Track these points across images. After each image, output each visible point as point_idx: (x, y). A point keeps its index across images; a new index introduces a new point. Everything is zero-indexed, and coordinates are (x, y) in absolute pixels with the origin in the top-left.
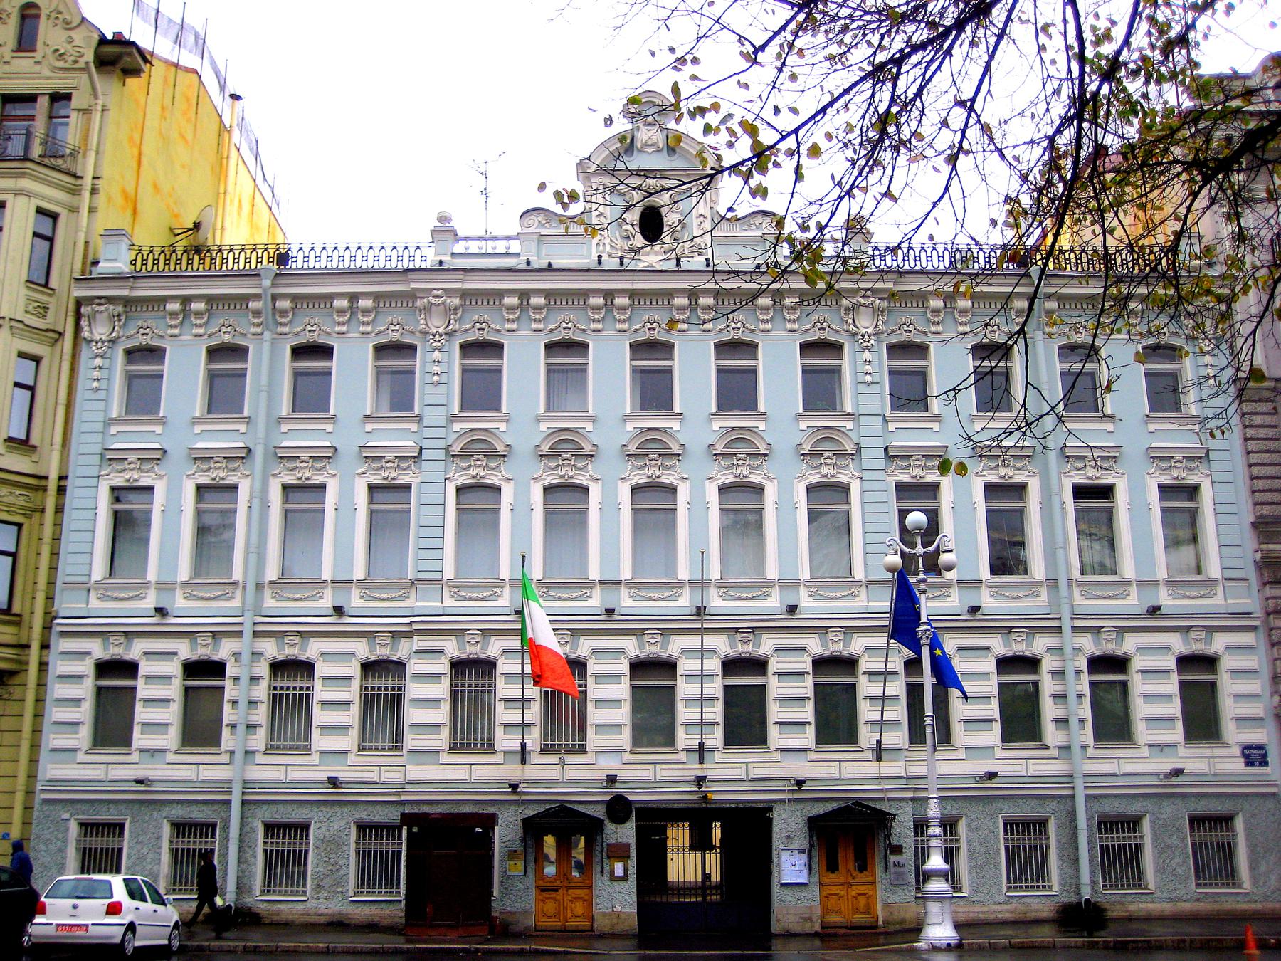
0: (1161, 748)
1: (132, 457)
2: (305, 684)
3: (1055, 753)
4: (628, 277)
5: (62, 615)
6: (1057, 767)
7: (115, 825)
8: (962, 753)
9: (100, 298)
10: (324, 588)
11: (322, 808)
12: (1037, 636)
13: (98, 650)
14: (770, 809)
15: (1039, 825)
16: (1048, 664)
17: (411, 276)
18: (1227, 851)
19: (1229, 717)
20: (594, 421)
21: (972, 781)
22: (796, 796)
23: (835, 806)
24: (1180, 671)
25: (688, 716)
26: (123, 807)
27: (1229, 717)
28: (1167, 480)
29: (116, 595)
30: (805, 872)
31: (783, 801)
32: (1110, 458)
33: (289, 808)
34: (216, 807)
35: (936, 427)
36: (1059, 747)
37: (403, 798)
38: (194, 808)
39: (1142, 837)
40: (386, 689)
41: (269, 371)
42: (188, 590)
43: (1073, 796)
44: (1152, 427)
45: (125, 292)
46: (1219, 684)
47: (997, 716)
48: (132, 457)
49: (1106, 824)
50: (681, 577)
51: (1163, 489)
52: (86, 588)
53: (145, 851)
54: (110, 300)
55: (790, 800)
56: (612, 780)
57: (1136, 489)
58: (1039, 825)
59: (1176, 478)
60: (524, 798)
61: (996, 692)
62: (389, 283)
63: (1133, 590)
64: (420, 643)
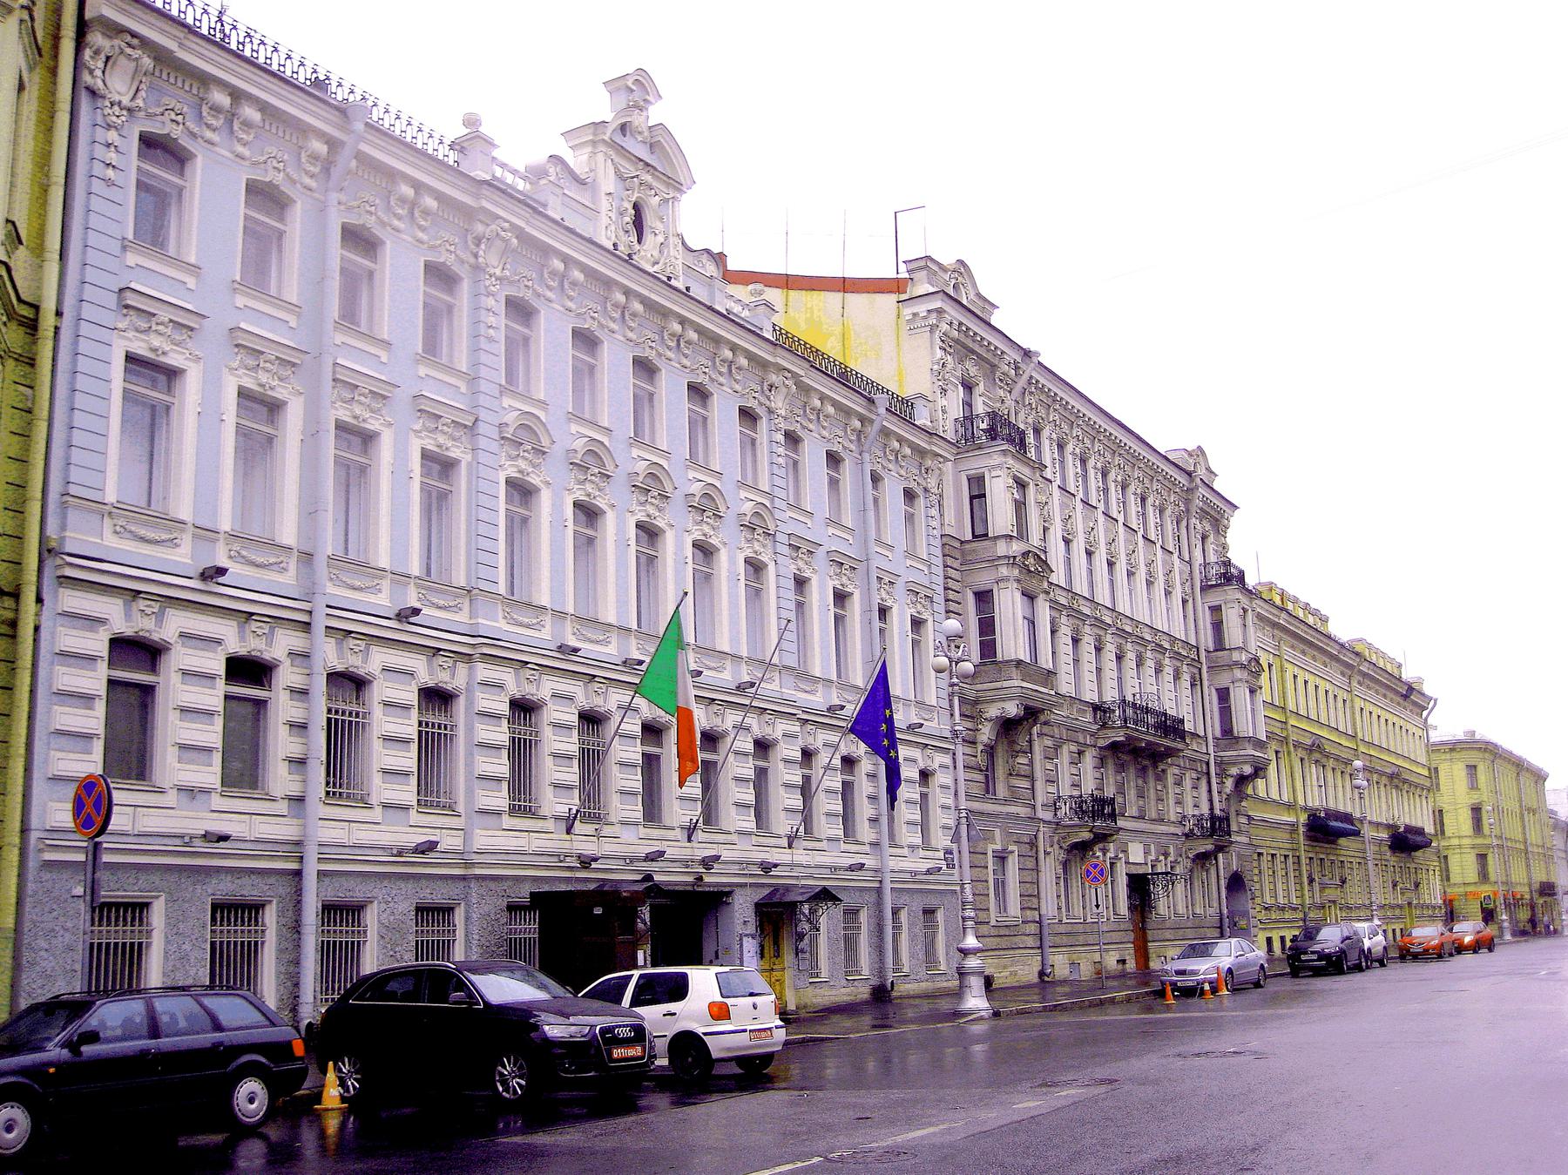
0: (190, 792)
1: (164, 315)
2: (355, 708)
3: (282, 807)
4: (627, 270)
5: (67, 550)
6: (284, 830)
7: (134, 906)
8: (171, 798)
9: (134, 35)
10: (183, 530)
11: (386, 883)
12: (170, 612)
13: (120, 619)
14: (729, 894)
15: (251, 910)
16: (287, 676)
17: (935, 440)
18: (251, 952)
19: (281, 754)
20: (198, 276)
21: (178, 841)
22: (579, 875)
23: (592, 886)
24: (112, 664)
25: (624, 783)
26: (156, 878)
27: (170, 741)
28: (249, 383)
29: (142, 532)
30: (43, 996)
31: (745, 885)
32: (186, 326)
33: (351, 883)
34: (272, 880)
35: (191, 282)
36: (290, 799)
37: (470, 872)
38: (246, 880)
39: (149, 932)
40: (344, 713)
41: (479, 315)
42: (236, 547)
43: (298, 874)
44: (241, 301)
45: (172, 45)
46: (271, 706)
47: (101, 731)
48: (164, 315)
49: (332, 911)
50: (183, 516)
51: (243, 394)
52: (98, 507)
53: (187, 947)
54: (145, 43)
55: (751, 885)
56: (767, 867)
57: (212, 385)
58: (251, 910)
59: (155, 350)
60: (478, 871)
61: (103, 692)
62: (454, 186)
63: (386, 584)
64: (484, 672)
